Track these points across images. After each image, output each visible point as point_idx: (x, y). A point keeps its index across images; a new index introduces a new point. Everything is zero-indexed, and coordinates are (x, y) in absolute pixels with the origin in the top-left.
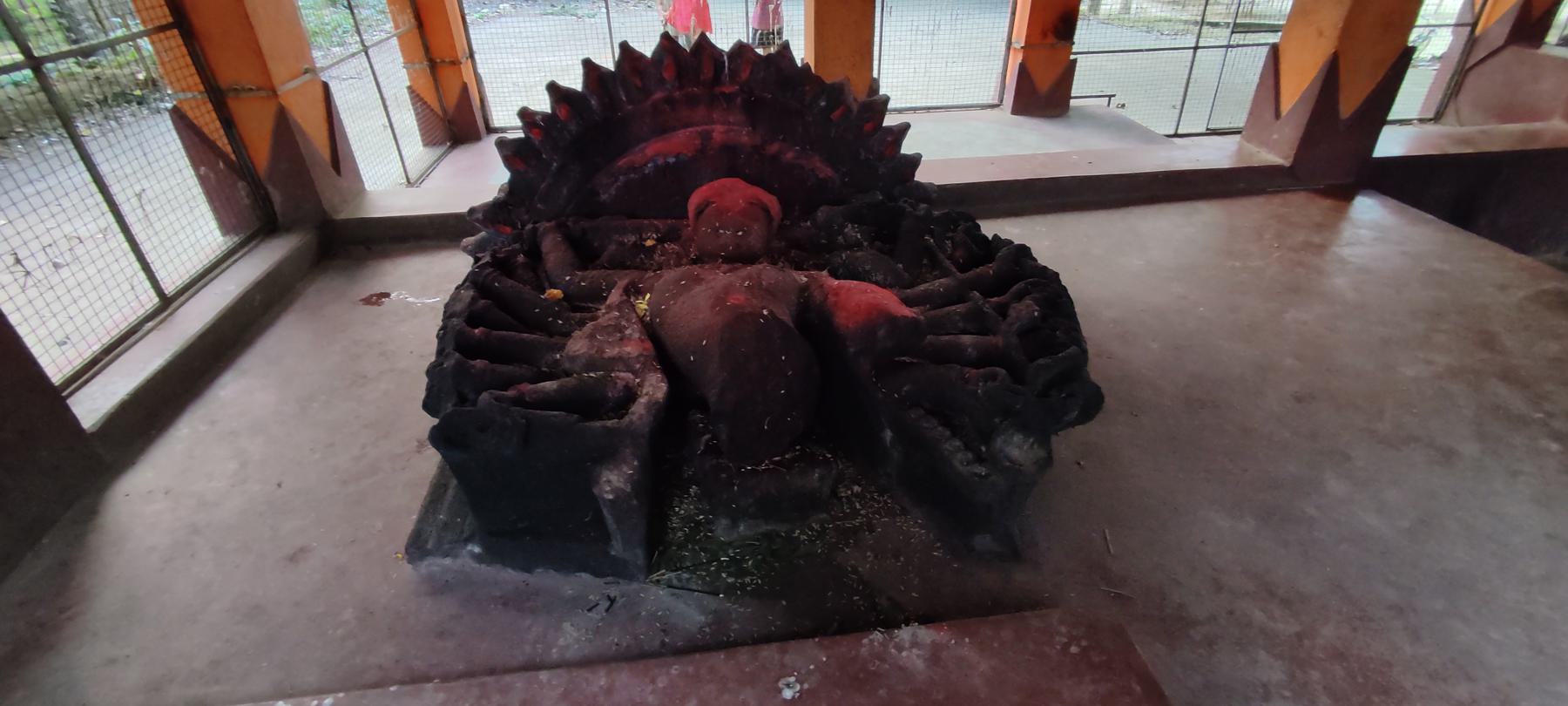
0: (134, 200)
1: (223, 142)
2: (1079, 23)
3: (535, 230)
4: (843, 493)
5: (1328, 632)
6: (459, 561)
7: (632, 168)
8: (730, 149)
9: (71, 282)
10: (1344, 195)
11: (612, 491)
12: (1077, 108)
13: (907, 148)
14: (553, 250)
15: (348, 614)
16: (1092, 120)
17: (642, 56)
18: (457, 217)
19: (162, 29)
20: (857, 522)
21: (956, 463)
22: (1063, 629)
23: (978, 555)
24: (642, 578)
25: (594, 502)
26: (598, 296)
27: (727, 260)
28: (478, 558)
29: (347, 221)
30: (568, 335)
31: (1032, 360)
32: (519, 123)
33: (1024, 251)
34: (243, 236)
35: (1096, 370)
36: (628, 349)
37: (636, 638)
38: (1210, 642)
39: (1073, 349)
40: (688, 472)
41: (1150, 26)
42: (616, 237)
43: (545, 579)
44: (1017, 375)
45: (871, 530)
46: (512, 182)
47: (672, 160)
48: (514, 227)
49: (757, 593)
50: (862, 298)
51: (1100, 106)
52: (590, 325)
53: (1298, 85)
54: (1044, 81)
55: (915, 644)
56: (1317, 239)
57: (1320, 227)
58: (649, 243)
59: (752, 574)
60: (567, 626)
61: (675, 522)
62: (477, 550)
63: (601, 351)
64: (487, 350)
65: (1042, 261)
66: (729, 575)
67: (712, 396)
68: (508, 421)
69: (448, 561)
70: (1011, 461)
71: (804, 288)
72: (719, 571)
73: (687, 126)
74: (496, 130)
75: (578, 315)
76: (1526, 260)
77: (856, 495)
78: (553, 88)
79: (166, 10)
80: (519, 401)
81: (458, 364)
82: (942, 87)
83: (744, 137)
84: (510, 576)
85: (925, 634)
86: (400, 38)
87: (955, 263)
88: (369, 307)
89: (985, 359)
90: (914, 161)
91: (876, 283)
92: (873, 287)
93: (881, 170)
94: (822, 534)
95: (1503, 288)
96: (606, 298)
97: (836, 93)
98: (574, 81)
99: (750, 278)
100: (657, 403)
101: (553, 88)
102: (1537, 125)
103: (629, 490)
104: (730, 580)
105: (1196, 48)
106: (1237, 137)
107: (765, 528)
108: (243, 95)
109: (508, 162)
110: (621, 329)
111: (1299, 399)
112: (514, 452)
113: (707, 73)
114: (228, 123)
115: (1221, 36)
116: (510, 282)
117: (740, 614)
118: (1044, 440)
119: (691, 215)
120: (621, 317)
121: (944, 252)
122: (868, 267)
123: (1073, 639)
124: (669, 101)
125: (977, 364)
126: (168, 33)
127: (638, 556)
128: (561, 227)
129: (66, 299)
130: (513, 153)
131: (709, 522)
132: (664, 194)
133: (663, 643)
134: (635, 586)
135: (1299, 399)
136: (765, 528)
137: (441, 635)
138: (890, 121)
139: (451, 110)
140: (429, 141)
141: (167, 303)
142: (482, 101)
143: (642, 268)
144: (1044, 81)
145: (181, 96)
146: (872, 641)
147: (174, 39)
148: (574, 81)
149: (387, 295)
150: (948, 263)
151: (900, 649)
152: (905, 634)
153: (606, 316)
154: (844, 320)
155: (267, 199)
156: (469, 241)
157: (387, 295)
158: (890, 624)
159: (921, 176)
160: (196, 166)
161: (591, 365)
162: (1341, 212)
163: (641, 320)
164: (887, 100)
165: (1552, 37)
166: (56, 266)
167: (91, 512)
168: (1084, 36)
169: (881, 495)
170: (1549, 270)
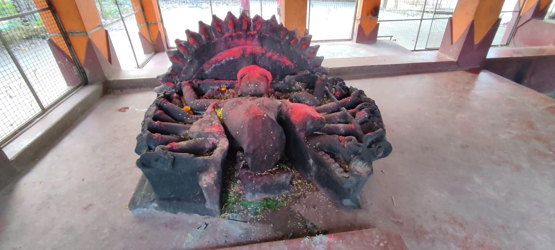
0: (33, 74)
1: (67, 52)
2: (380, 11)
3: (180, 84)
4: (295, 183)
5: (476, 236)
6: (150, 209)
7: (217, 61)
9: (17, 103)
10: (476, 71)
11: (206, 184)
14: (188, 92)
15: (106, 230)
16: (384, 45)
17: (220, 21)
19: (44, 10)
20: (299, 194)
21: (336, 172)
22: (377, 236)
24: (218, 216)
26: (203, 109)
27: (252, 95)
28: (156, 208)
29: (114, 81)
30: (191, 124)
31: (365, 134)
33: (361, 93)
34: (75, 86)
35: (389, 137)
37: (216, 239)
38: (432, 241)
39: (380, 129)
40: (237, 175)
41: (404, 12)
42: (211, 87)
43: (182, 216)
44: (360, 140)
48: (174, 83)
49: (262, 222)
50: (303, 110)
52: (200, 120)
53: (460, 31)
54: (367, 32)
55: (321, 243)
56: (467, 88)
57: (468, 83)
58: (223, 89)
59: (260, 214)
60: (189, 235)
61: (231, 194)
62: (156, 205)
63: (203, 130)
64: (164, 122)
66: (251, 214)
67: (245, 148)
68: (166, 157)
69: (145, 209)
70: (358, 172)
71: (280, 106)
72: (247, 214)
75: (196, 116)
76: (542, 95)
77: (299, 184)
78: (188, 32)
79: (46, 3)
80: (171, 150)
82: (331, 35)
84: (168, 215)
86: (136, 14)
88: (121, 113)
89: (347, 133)
91: (307, 104)
92: (306, 106)
94: (286, 198)
95: (535, 105)
96: (206, 110)
97: (292, 35)
98: (196, 29)
101: (188, 32)
102: (544, 47)
103: (213, 183)
104: (252, 216)
105: (422, 19)
106: (437, 51)
107: (265, 196)
108: (75, 34)
109: (172, 59)
111: (463, 147)
112: (169, 168)
113: (245, 27)
114: (69, 45)
115: (431, 16)
117: (257, 230)
118: (370, 164)
119: (238, 78)
121: (332, 93)
123: (381, 240)
124: (231, 37)
125: (345, 135)
126: (47, 11)
127: (217, 208)
128: (190, 83)
129: (15, 109)
130: (175, 57)
131: (244, 194)
132: (229, 72)
133: (226, 242)
134: (215, 219)
135: (463, 147)
136: (265, 196)
137: (141, 238)
139: (154, 41)
140: (146, 52)
141: (44, 111)
142: (166, 37)
145: (52, 35)
147: (49, 13)
148: (196, 29)
149: (128, 108)
150: (333, 97)
151: (315, 245)
152: (317, 238)
153: (206, 116)
154: (294, 119)
155: (84, 73)
157: (128, 108)
159: (323, 65)
160: (57, 61)
161: (199, 136)
162: (475, 79)
163: (219, 118)
164: (311, 37)
165: (546, 17)
166: (11, 97)
167: (11, 191)
168: (382, 15)
169: (309, 183)
170: (551, 99)
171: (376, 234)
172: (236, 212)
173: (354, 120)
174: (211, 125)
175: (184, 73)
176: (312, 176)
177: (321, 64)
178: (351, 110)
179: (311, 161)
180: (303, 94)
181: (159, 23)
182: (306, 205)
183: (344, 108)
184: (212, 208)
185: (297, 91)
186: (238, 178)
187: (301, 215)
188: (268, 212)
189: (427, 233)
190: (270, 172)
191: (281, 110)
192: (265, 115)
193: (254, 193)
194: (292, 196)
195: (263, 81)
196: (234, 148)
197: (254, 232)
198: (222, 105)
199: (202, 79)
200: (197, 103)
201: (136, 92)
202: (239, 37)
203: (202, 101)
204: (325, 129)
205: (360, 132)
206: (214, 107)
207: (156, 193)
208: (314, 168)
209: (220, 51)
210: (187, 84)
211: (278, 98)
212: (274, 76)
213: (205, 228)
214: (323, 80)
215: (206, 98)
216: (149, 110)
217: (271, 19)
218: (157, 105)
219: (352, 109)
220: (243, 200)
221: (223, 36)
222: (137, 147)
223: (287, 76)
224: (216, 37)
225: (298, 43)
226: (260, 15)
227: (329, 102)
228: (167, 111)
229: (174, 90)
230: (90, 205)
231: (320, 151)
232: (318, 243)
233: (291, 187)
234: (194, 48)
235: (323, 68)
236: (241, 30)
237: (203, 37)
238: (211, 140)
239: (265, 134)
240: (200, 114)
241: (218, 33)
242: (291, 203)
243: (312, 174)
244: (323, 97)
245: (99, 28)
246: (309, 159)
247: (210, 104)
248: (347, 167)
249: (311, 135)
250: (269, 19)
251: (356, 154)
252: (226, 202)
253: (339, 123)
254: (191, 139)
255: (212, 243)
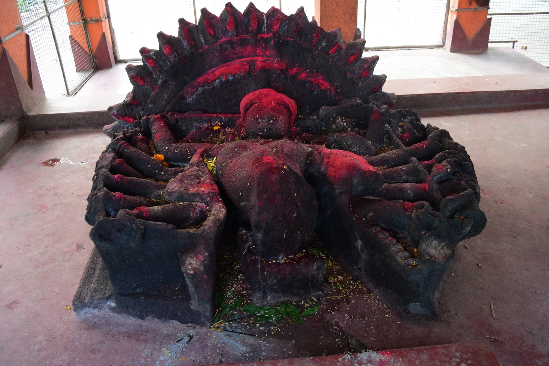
3: (148, 119)
4: (332, 280)
6: (103, 311)
7: (207, 82)
8: (266, 71)
11: (193, 269)
12: (492, 49)
13: (377, 71)
14: (158, 131)
16: (501, 56)
17: (214, 17)
18: (100, 114)
20: (340, 297)
22: (458, 354)
23: (413, 301)
25: (181, 275)
27: (262, 137)
28: (113, 309)
29: (35, 117)
30: (167, 181)
32: (140, 56)
33: (445, 134)
36: (202, 189)
39: (469, 190)
40: (237, 266)
42: (196, 124)
43: (152, 323)
44: (435, 205)
45: (348, 302)
46: (134, 91)
47: (231, 78)
49: (278, 336)
50: (344, 159)
51: (507, 48)
52: (180, 175)
54: (471, 32)
55: (369, 361)
58: (216, 128)
59: (275, 325)
60: (164, 350)
61: (229, 294)
62: (113, 304)
63: (186, 189)
64: (121, 184)
65: (456, 140)
67: (254, 218)
69: (96, 311)
71: (310, 154)
72: (254, 323)
73: (240, 58)
74: (124, 61)
75: (173, 169)
78: (161, 36)
81: (106, 194)
82: (404, 34)
83: (275, 62)
84: (130, 321)
85: (376, 356)
86: (67, 8)
87: (404, 141)
88: (48, 167)
89: (419, 197)
90: (382, 80)
93: (361, 85)
96: (190, 160)
98: (173, 31)
99: (277, 147)
100: (219, 220)
101: (161, 36)
104: (261, 328)
109: (133, 79)
110: (198, 177)
112: (139, 247)
113: (253, 27)
116: (134, 149)
119: (242, 111)
120: (199, 170)
122: (349, 143)
124: (230, 42)
127: (206, 309)
128: (163, 118)
130: (136, 75)
131: (249, 295)
134: (204, 329)
137: (93, 351)
138: (365, 55)
139: (95, 50)
140: (80, 69)
142: (113, 43)
143: (212, 142)
144: (471, 32)
146: (344, 359)
148: (173, 31)
149: (58, 160)
150: (398, 141)
152: (364, 356)
153: (189, 170)
156: (107, 127)
157: (58, 160)
158: (355, 351)
159: (386, 89)
161: (181, 198)
163: (211, 172)
164: (364, 42)
169: (355, 281)
171: (457, 351)
172: (235, 320)
173: (429, 178)
174: (199, 183)
175: (151, 103)
176: (360, 269)
177: (381, 88)
178: (426, 162)
179: (359, 243)
180: (348, 137)
181: (104, 19)
182: (349, 313)
183: (414, 159)
184: (200, 309)
185: (340, 131)
186: (240, 271)
187: (341, 330)
188: (288, 322)
189: (541, 356)
190: (292, 259)
191: (311, 161)
192: (285, 167)
193: (265, 293)
194: (327, 300)
195: (282, 114)
196: (235, 219)
197: (265, 351)
198: (215, 152)
199: (181, 112)
200: (175, 149)
201: (70, 135)
202: (243, 43)
203: (182, 145)
204: (383, 190)
205: (438, 195)
206: (202, 155)
207: (113, 283)
208: (364, 256)
209: (212, 66)
210: (158, 119)
211: (307, 142)
212: (300, 107)
213: (188, 342)
214: (382, 114)
215: (188, 142)
216: (101, 158)
217: (297, 14)
218: (114, 150)
219: (428, 160)
220: (248, 304)
221: (217, 41)
222: (89, 209)
223: (323, 108)
224: (206, 43)
225: (343, 52)
226: (277, 7)
227: (392, 149)
228: (129, 160)
229: (137, 129)
230: (14, 302)
231: (373, 226)
232: (365, 362)
233: (325, 287)
234: (170, 61)
235: (385, 94)
236: (247, 33)
237: (185, 44)
238: (199, 205)
239: (285, 196)
240: (179, 166)
241: (209, 37)
242: (325, 311)
243: (361, 265)
244: (381, 142)
245: (18, 32)
246: (356, 240)
247: (195, 151)
248: (415, 250)
249: (358, 202)
250: (294, 13)
251: (429, 228)
252: (219, 305)
253: (406, 182)
254: (167, 203)
255: (200, 362)
